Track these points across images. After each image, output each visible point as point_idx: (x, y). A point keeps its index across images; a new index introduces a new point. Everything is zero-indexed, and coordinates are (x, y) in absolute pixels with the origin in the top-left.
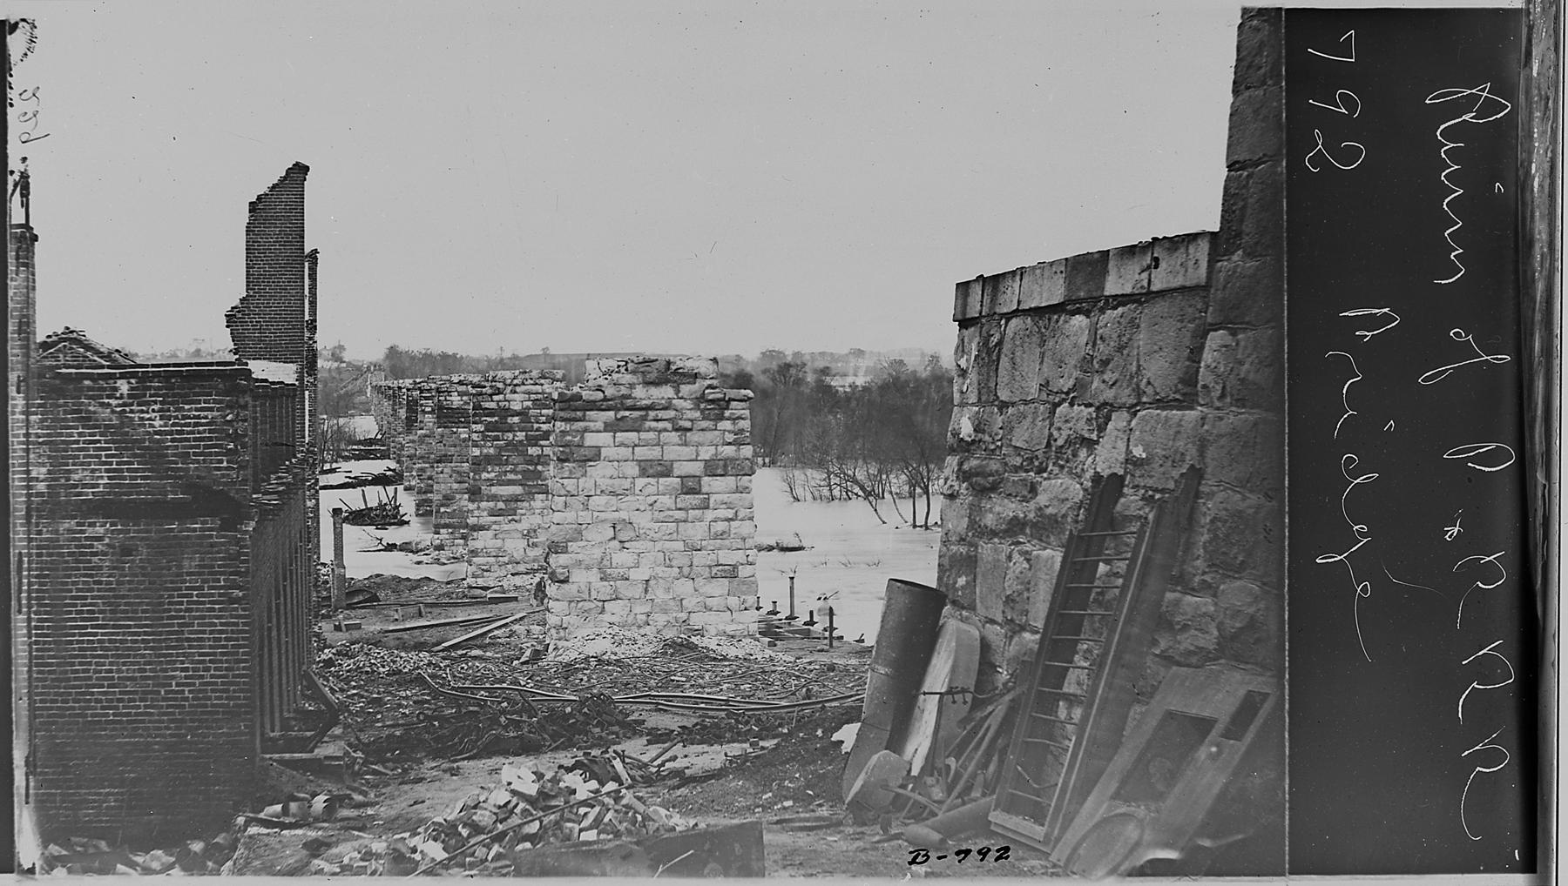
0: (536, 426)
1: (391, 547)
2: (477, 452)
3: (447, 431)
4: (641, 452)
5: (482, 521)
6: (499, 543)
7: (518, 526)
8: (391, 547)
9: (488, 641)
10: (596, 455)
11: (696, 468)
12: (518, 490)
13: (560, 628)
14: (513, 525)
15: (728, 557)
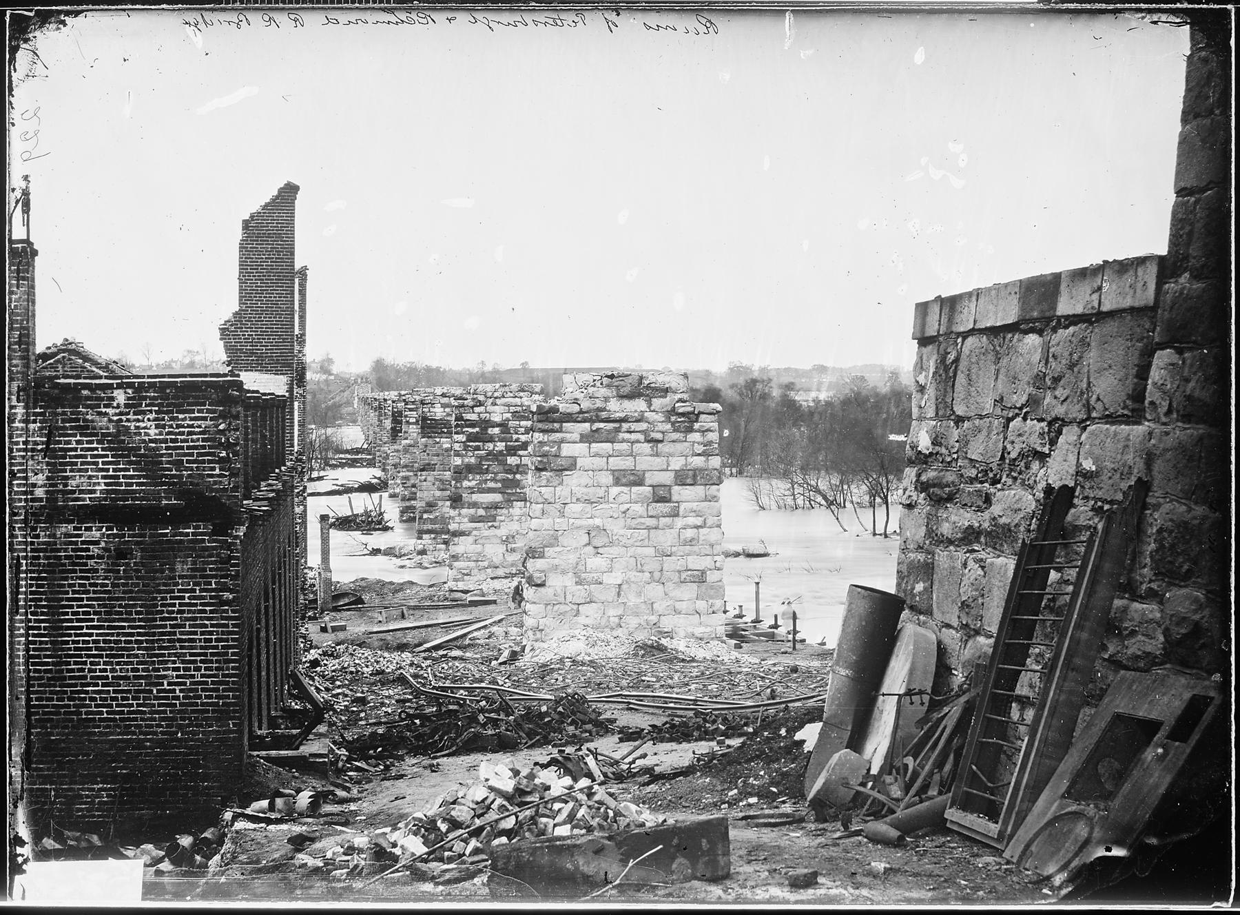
0: (515, 437)
1: (376, 552)
3: (430, 441)
4: (616, 463)
6: (479, 548)
7: (497, 532)
8: (376, 552)
9: (467, 642)
10: (572, 465)
11: (667, 478)
12: (497, 497)
13: (537, 629)
14: (493, 532)
15: (697, 563)
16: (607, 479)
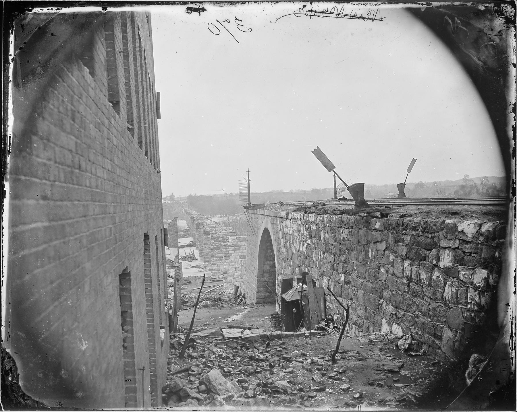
0: (226, 240)
1: (193, 267)
2: (212, 247)
3: (206, 237)
4: (240, 254)
5: (214, 263)
8: (193, 267)
9: (216, 290)
13: (226, 288)
16: (239, 257)
